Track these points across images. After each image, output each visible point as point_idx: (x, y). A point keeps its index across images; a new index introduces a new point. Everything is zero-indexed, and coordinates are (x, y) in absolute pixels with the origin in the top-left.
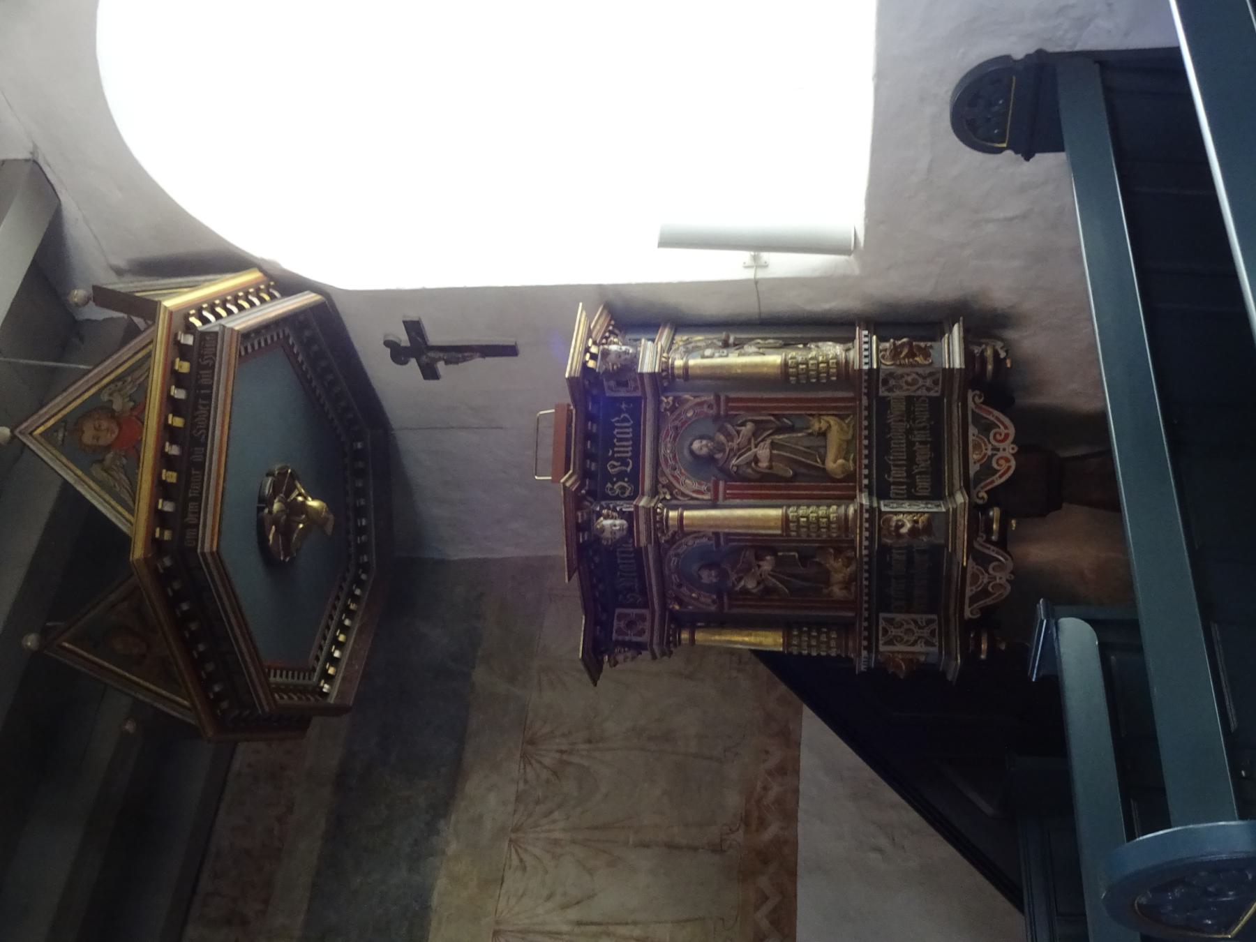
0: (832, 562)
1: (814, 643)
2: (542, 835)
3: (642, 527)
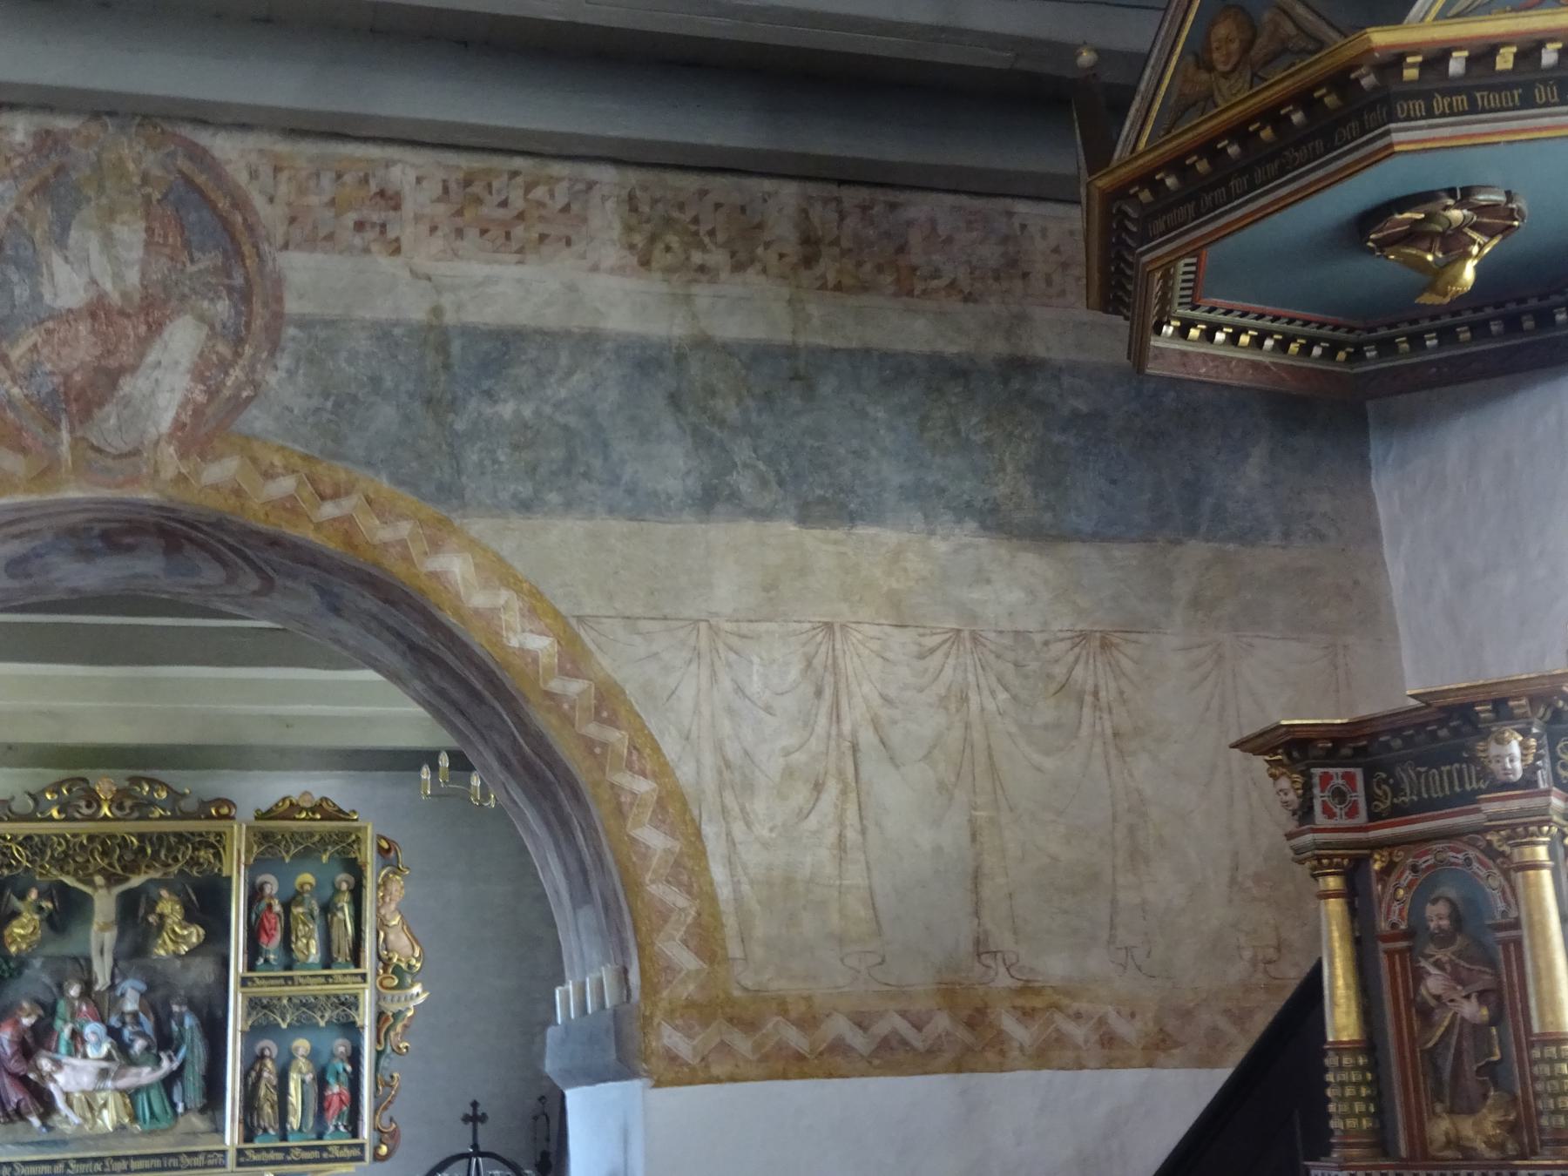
0: (1493, 1118)
1: (1349, 1092)
2: (971, 678)
3: (1515, 805)
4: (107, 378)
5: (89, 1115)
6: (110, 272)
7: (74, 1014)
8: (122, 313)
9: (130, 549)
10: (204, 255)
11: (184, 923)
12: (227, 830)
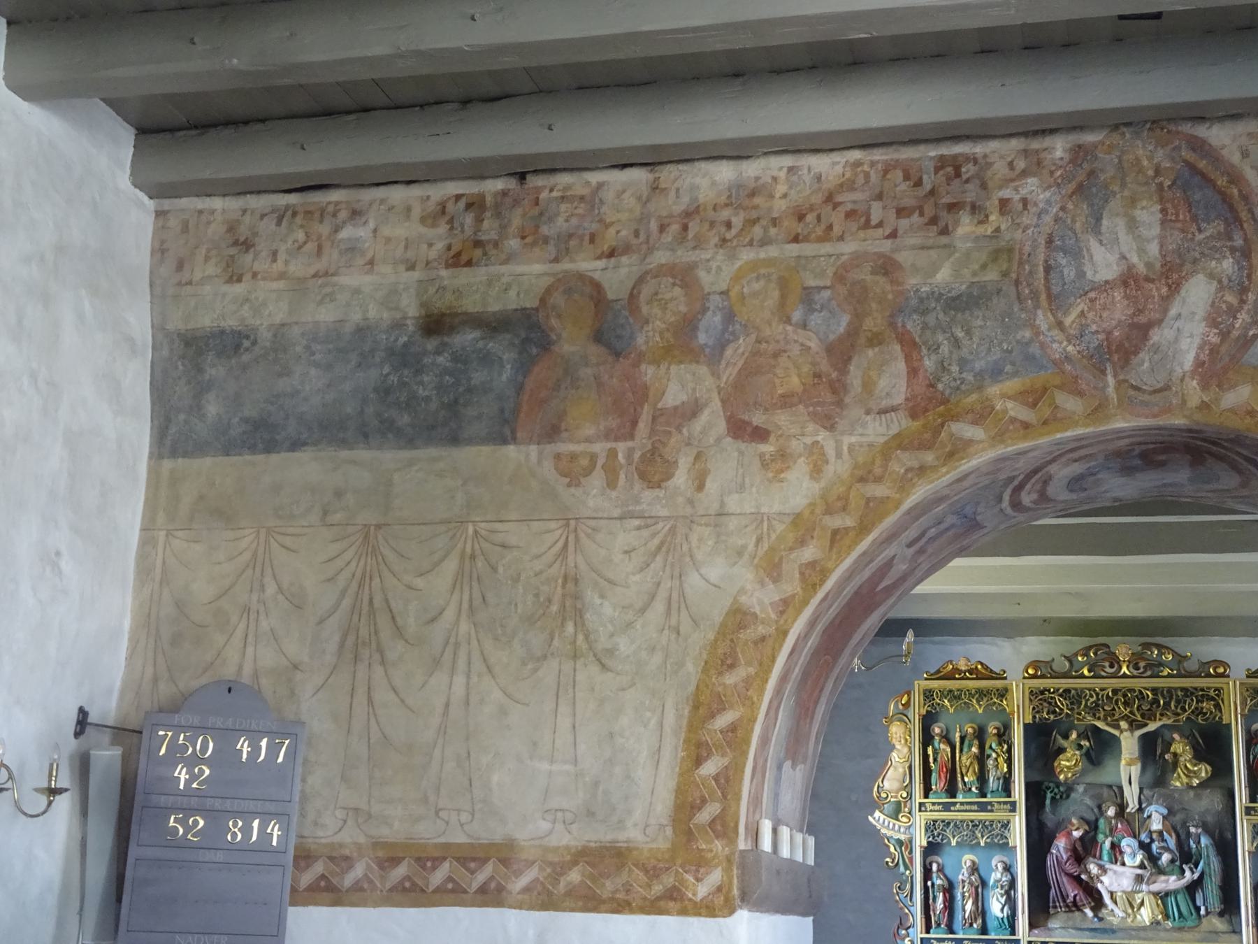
4: (1140, 331)
5: (1130, 911)
6: (1135, 247)
7: (1112, 831)
8: (1148, 279)
9: (1161, 465)
10: (1209, 224)
11: (1194, 761)
12: (1225, 686)
